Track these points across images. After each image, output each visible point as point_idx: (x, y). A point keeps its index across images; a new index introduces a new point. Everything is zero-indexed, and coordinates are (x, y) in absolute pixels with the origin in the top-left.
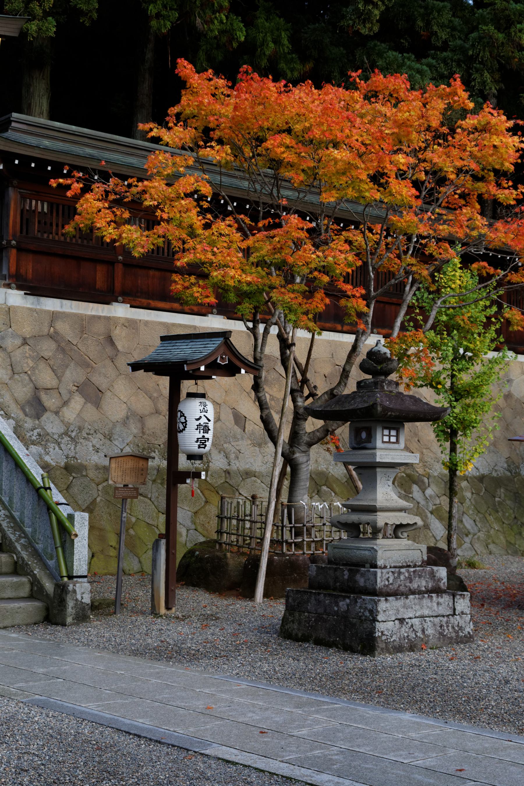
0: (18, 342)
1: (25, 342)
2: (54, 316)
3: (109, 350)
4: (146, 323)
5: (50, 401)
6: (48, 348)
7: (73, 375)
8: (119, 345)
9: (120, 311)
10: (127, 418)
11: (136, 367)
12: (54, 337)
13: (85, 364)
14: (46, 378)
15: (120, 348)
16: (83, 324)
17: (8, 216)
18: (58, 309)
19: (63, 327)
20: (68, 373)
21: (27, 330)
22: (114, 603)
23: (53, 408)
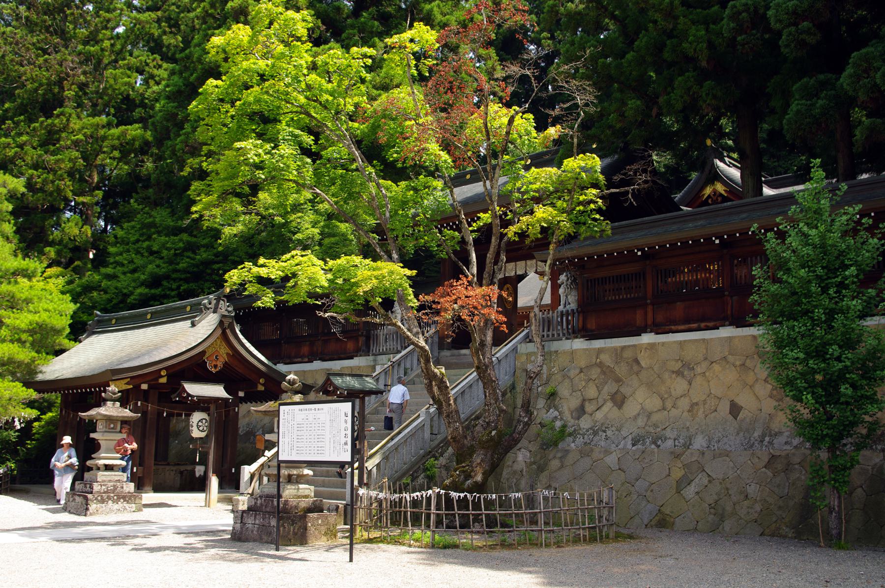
0: (578, 371)
1: (581, 371)
2: (600, 351)
3: (635, 368)
4: (663, 344)
5: (589, 408)
6: (595, 373)
7: (610, 388)
8: (643, 364)
9: (647, 338)
10: (638, 415)
11: (351, 560)
12: (601, 365)
13: (618, 380)
14: (592, 392)
15: (643, 365)
16: (618, 353)
17: (267, 549)
18: (603, 346)
19: (605, 358)
20: (606, 387)
21: (583, 364)
22: (678, 492)
23: (590, 412)
